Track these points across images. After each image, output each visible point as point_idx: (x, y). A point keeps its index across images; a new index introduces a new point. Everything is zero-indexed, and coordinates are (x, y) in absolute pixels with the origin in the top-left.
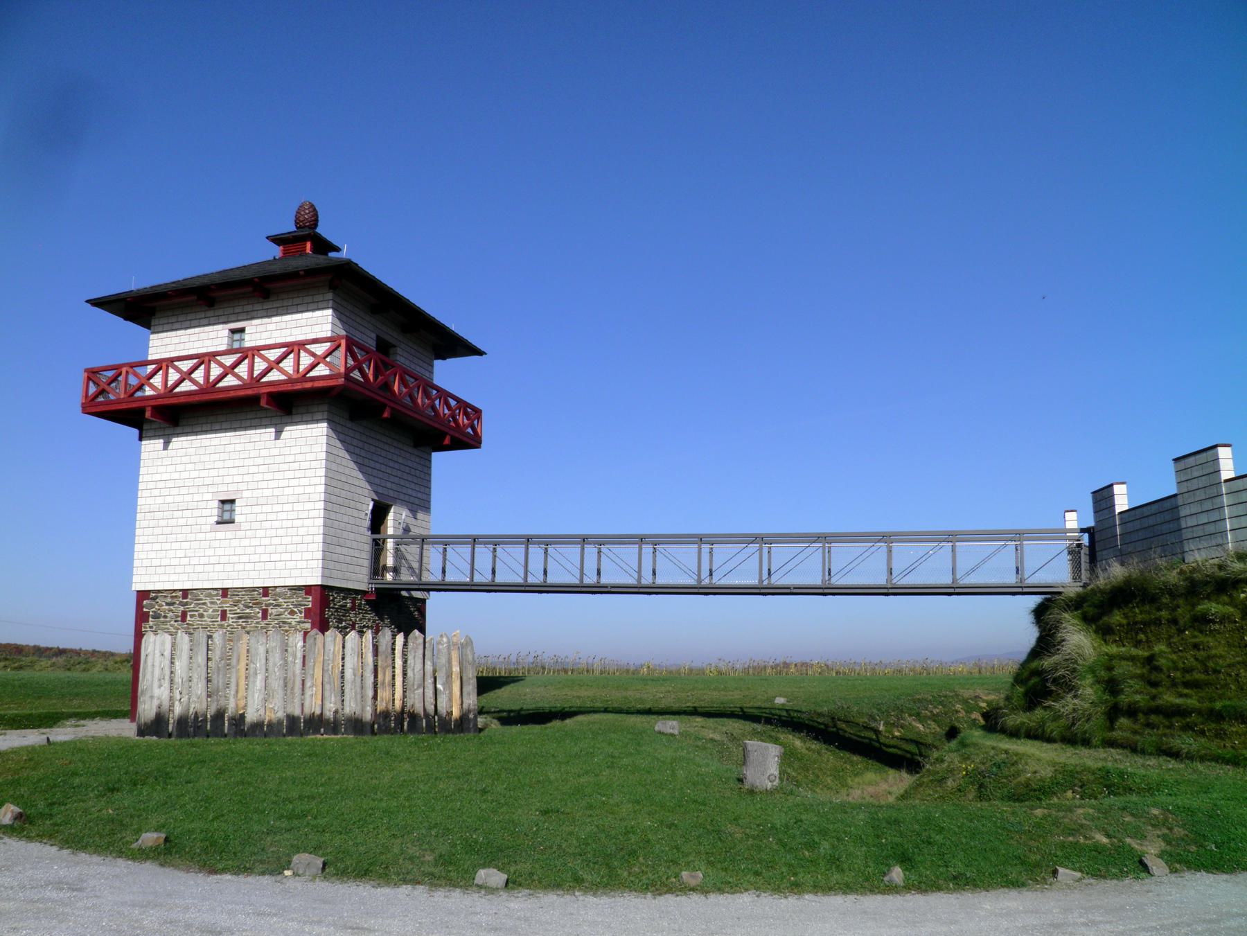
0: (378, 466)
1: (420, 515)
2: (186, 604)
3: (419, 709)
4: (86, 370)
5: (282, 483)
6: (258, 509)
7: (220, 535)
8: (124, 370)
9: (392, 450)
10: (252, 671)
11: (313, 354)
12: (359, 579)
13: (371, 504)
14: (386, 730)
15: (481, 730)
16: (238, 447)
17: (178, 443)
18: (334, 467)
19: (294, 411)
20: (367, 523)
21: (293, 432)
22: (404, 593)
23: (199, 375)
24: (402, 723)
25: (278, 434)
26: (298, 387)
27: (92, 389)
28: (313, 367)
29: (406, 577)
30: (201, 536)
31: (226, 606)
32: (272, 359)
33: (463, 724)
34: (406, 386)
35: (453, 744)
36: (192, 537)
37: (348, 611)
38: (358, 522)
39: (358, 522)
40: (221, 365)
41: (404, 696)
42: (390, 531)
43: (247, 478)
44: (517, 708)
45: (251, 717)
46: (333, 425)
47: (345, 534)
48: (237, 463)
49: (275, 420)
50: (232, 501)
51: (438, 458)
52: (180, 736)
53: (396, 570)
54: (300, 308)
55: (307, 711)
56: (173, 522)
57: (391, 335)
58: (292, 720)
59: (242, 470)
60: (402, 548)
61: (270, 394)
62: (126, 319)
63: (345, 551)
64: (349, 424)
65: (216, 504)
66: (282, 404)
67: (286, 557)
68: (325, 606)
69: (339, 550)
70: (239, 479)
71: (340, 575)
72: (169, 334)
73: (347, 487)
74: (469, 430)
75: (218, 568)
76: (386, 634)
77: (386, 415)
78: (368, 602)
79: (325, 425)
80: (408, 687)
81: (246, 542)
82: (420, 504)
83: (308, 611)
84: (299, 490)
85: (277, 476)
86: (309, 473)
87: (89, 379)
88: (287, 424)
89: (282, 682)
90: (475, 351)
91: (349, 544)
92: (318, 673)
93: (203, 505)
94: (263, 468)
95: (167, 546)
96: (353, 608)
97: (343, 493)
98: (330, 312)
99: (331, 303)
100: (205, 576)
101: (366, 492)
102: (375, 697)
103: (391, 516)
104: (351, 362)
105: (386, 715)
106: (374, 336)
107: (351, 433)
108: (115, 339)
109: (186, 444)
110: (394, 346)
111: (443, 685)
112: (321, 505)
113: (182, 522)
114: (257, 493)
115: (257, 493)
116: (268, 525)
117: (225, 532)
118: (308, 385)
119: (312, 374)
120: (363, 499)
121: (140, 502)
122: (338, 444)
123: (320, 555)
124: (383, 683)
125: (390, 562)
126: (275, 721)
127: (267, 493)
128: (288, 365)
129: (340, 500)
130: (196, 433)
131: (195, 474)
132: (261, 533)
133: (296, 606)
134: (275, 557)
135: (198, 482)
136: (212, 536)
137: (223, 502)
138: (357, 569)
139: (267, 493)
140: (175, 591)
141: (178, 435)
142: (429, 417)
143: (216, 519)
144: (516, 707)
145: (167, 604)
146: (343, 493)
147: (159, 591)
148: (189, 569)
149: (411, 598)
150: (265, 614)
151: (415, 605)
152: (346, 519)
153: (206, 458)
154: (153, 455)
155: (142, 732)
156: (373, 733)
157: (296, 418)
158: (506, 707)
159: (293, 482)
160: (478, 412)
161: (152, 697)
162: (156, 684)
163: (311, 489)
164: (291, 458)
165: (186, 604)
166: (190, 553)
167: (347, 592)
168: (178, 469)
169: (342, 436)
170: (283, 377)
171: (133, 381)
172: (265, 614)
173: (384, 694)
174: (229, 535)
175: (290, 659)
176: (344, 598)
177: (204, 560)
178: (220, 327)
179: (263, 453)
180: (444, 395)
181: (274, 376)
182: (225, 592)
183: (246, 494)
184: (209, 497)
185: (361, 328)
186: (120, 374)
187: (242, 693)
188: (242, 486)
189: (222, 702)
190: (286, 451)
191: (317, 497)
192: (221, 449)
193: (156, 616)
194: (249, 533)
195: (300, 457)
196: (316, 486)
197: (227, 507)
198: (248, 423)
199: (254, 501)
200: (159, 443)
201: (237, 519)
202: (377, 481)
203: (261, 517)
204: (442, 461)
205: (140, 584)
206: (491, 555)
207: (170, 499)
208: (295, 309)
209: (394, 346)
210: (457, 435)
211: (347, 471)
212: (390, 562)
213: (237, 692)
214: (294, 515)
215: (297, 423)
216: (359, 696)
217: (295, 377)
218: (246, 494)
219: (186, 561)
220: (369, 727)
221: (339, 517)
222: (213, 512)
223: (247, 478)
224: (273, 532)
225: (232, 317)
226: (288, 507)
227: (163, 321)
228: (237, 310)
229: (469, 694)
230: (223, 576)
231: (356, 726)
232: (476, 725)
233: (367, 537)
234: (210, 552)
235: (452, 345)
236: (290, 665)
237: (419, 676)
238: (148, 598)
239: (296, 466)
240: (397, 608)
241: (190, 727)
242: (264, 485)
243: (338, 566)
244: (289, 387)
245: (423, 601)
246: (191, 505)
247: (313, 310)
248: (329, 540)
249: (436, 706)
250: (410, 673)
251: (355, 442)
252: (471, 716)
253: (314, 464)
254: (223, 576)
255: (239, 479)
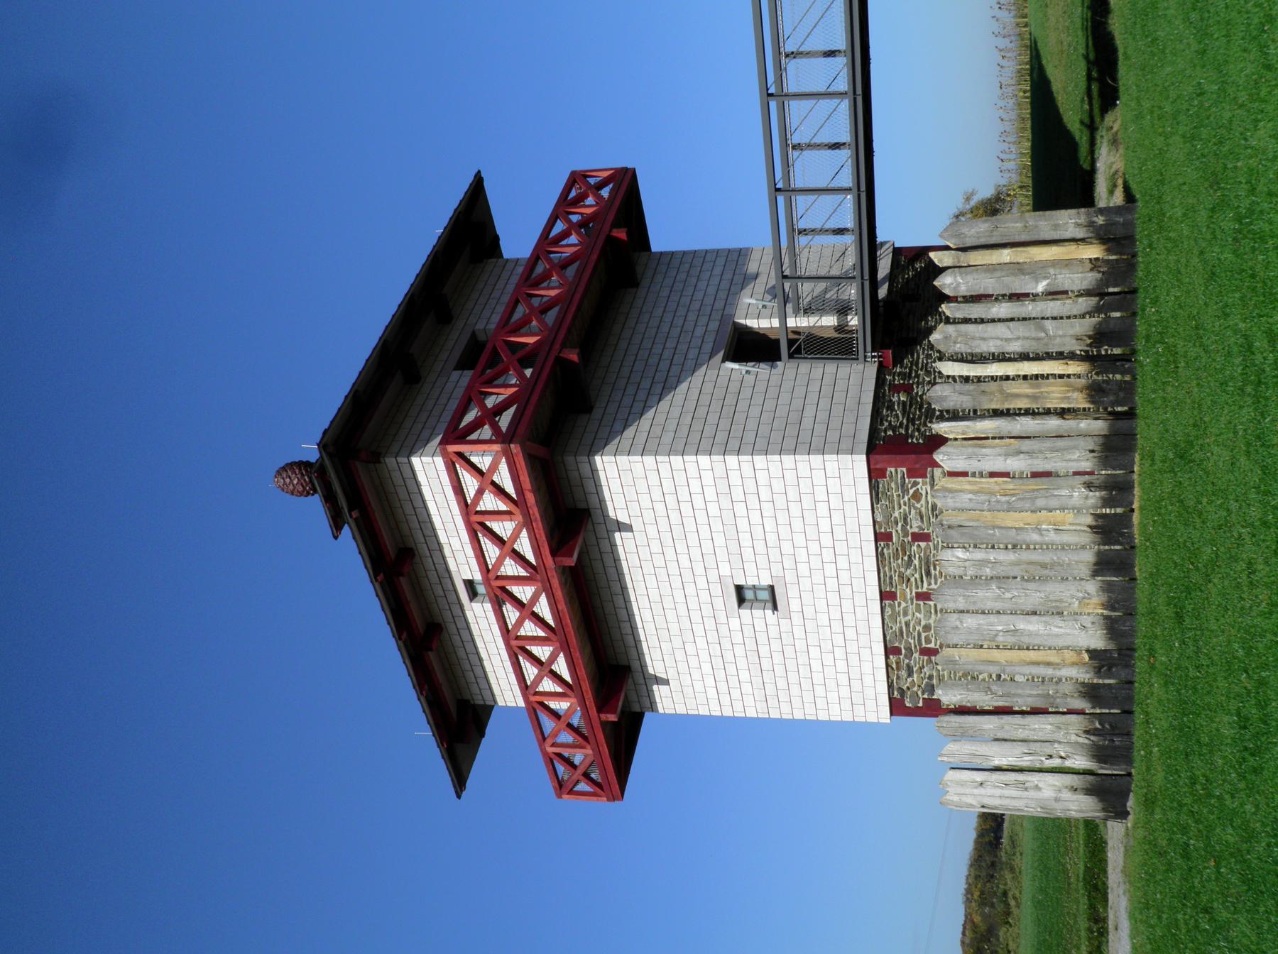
0: (667, 354)
1: (752, 268)
2: (909, 649)
3: (1085, 326)
4: (559, 796)
5: (701, 517)
6: (748, 553)
7: (795, 605)
8: (550, 750)
9: (641, 328)
10: (1011, 640)
11: (480, 492)
12: (856, 379)
13: (730, 365)
14: (1128, 390)
15: (1129, 197)
16: (651, 582)
17: (655, 663)
18: (667, 439)
19: (582, 506)
20: (763, 369)
21: (617, 504)
22: (883, 292)
23: (543, 652)
24: (1112, 356)
25: (621, 527)
26: (535, 512)
27: (583, 786)
28: (500, 491)
29: (851, 292)
30: (799, 632)
31: (910, 593)
32: (497, 552)
33: (1117, 236)
34: (525, 321)
35: (1154, 259)
36: (801, 645)
37: (912, 400)
38: (761, 387)
39: (761, 387)
40: (520, 623)
41: (1060, 356)
42: (776, 323)
43: (699, 569)
44: (1082, 65)
45: (1096, 639)
46: (597, 446)
47: (782, 411)
48: (677, 583)
49: (601, 531)
50: (739, 589)
51: (660, 240)
52: (1129, 761)
53: (843, 310)
54: (418, 504)
55: (1087, 538)
56: (779, 671)
57: (454, 342)
58: (1103, 565)
59: (687, 576)
60: (804, 302)
61: (554, 553)
62: (483, 735)
63: (809, 412)
64: (597, 413)
65: (745, 612)
66: (572, 529)
67: (822, 509)
68: (899, 443)
69: (807, 423)
70: (702, 582)
71: (850, 418)
72: (492, 681)
73: (701, 412)
74: (605, 193)
75: (847, 605)
76: (943, 396)
77: (574, 356)
78: (898, 360)
79: (598, 459)
80: (1041, 350)
81: (803, 569)
82: (732, 266)
83: (912, 473)
84: (710, 493)
85: (690, 526)
86: (681, 479)
87: (571, 792)
88: (605, 515)
89: (1032, 585)
90: (477, 187)
91: (797, 403)
92: (1012, 519)
93: (748, 631)
94: (681, 547)
95: (818, 678)
96: (908, 389)
97: (713, 418)
98: (415, 460)
99: (402, 460)
100: (862, 627)
101: (712, 374)
102: (1062, 413)
103: (752, 323)
104: (486, 432)
105: (1095, 391)
106: (456, 374)
107: (612, 409)
108: (505, 752)
109: (656, 655)
110: (474, 334)
111: (1037, 281)
112: (732, 460)
113: (778, 658)
114: (721, 554)
115: (721, 554)
116: (772, 538)
117: (789, 597)
118: (531, 498)
119: (510, 488)
120: (723, 381)
121: (751, 713)
122: (629, 432)
123: (816, 459)
124: (1034, 398)
125: (830, 321)
126: (1104, 598)
127: (720, 540)
128: (504, 528)
129: (724, 424)
130: (637, 642)
131: (701, 643)
132: (787, 547)
133: (905, 491)
134: (825, 525)
135: (712, 637)
136: (797, 618)
137: (741, 600)
138: (841, 385)
139: (720, 540)
140: (888, 666)
141: (643, 666)
142: (579, 273)
143: (769, 612)
144: (1082, 67)
145: (910, 674)
146: (713, 418)
147: (890, 686)
148: (852, 647)
149: (892, 277)
150: (918, 537)
151: (905, 268)
152: (755, 411)
153: (674, 628)
154: (678, 697)
155: (1122, 814)
156: (1131, 414)
157: (593, 500)
158: (1083, 84)
159: (698, 502)
160: (576, 178)
161: (1057, 800)
162: (1032, 794)
163: (708, 478)
164: (660, 507)
165: (909, 649)
166: (827, 646)
167: (880, 402)
168: (693, 661)
169: (618, 426)
170: (524, 533)
171: (566, 737)
172: (918, 537)
173: (1055, 396)
174: (793, 592)
175: (988, 571)
176: (891, 408)
177: (837, 627)
178: (469, 615)
179: (656, 547)
180: (546, 242)
181: (525, 546)
182: (886, 596)
183: (725, 570)
184: (735, 623)
185: (443, 400)
186: (559, 755)
187: (1052, 657)
188: (713, 576)
189: (1067, 688)
190: (648, 515)
191: (719, 468)
192: (657, 609)
193: (931, 689)
194: (788, 563)
195: (657, 495)
196: (700, 472)
197: (749, 595)
198: (612, 571)
199: (736, 560)
200: (659, 692)
201: (766, 582)
202: (692, 354)
203: (760, 547)
204: (666, 232)
205: (879, 711)
206: (807, 154)
207: (744, 676)
208: (420, 511)
209: (474, 334)
210: (611, 217)
211: (675, 412)
212: (830, 321)
213: (1048, 664)
214: (753, 501)
215: (602, 501)
216: (1060, 443)
217: (520, 518)
218: (725, 570)
219: (839, 653)
220: (1120, 424)
221: (752, 425)
222: (758, 616)
223: (699, 569)
224: (784, 532)
225: (452, 598)
226: (740, 509)
227: (475, 689)
228: (439, 592)
229: (1056, 227)
230: (860, 600)
231: (1116, 447)
232: (1118, 210)
233: (787, 371)
234: (823, 619)
235: (471, 229)
236: (1000, 571)
237: (1020, 329)
238: (902, 701)
239: (671, 500)
240: (903, 306)
241: (1113, 738)
242: (707, 546)
243: (835, 423)
244: (539, 525)
245: (897, 252)
246: (750, 644)
247: (418, 485)
248: (789, 443)
249: (1083, 316)
250: (1015, 347)
251: (627, 401)
252: (1100, 220)
253: (665, 472)
254: (860, 600)
255: (702, 582)
